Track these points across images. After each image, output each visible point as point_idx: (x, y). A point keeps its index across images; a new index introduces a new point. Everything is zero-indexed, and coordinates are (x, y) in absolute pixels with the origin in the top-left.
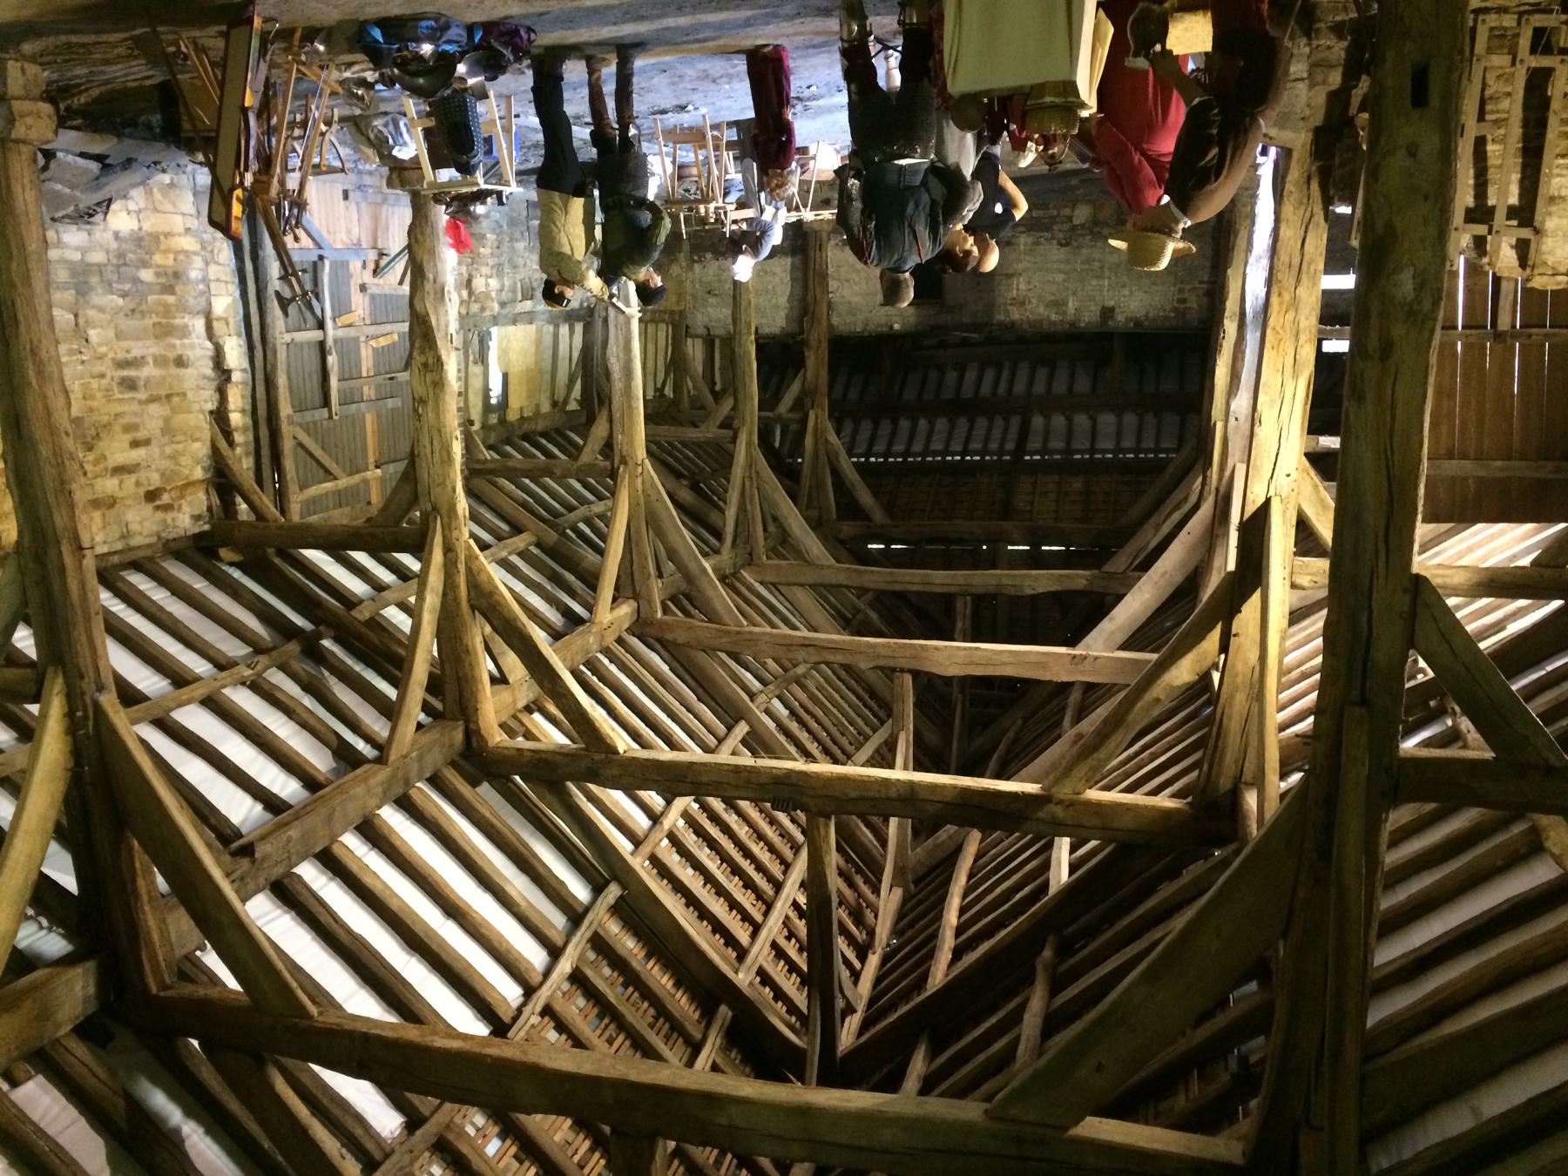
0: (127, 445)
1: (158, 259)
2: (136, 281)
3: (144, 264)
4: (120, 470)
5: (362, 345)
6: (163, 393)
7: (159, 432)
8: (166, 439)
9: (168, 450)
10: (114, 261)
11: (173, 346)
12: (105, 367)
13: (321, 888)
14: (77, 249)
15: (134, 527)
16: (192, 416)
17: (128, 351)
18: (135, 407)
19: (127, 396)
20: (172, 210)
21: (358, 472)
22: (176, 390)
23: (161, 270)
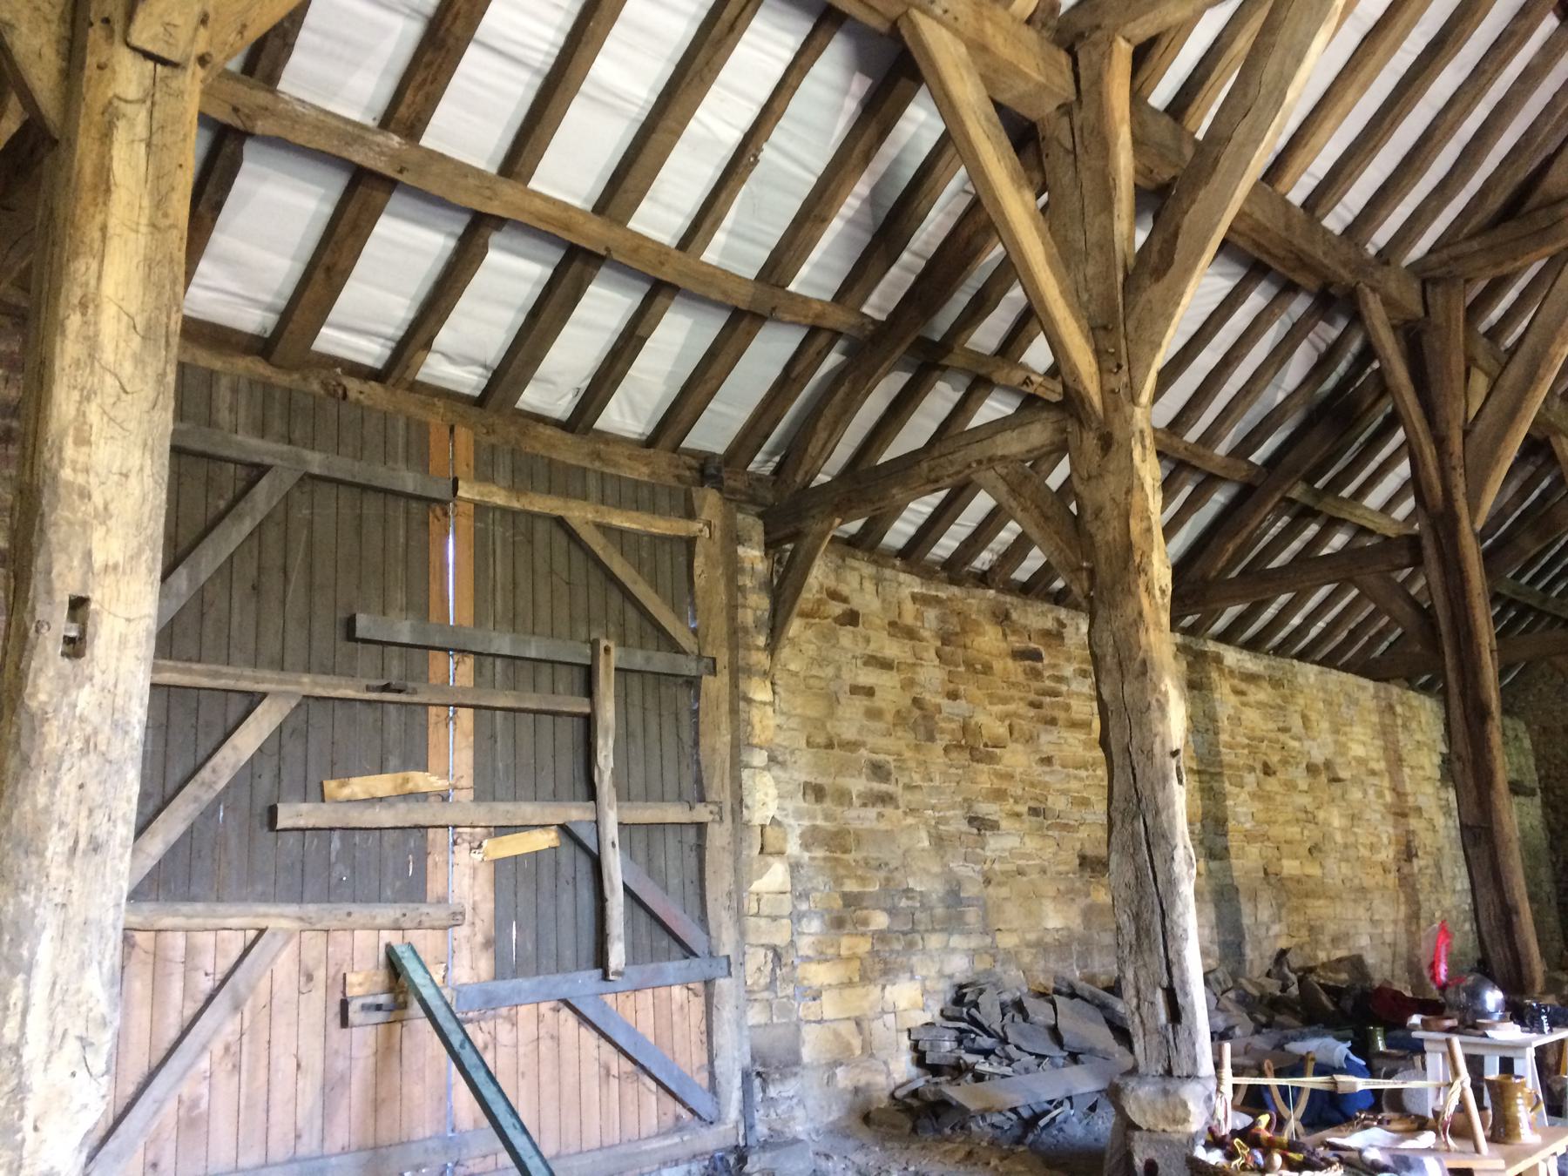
0: (878, 693)
1: (864, 946)
2: (892, 912)
3: (882, 936)
4: (886, 665)
5: (467, 781)
6: (837, 751)
7: (843, 700)
8: (833, 687)
9: (830, 671)
10: (918, 937)
11: (827, 817)
12: (904, 798)
13: (1350, 210)
14: (954, 950)
15: (869, 586)
16: (799, 711)
17: (881, 815)
18: (871, 740)
19: (881, 757)
20: (835, 1025)
21: (514, 513)
22: (822, 752)
23: (861, 929)
